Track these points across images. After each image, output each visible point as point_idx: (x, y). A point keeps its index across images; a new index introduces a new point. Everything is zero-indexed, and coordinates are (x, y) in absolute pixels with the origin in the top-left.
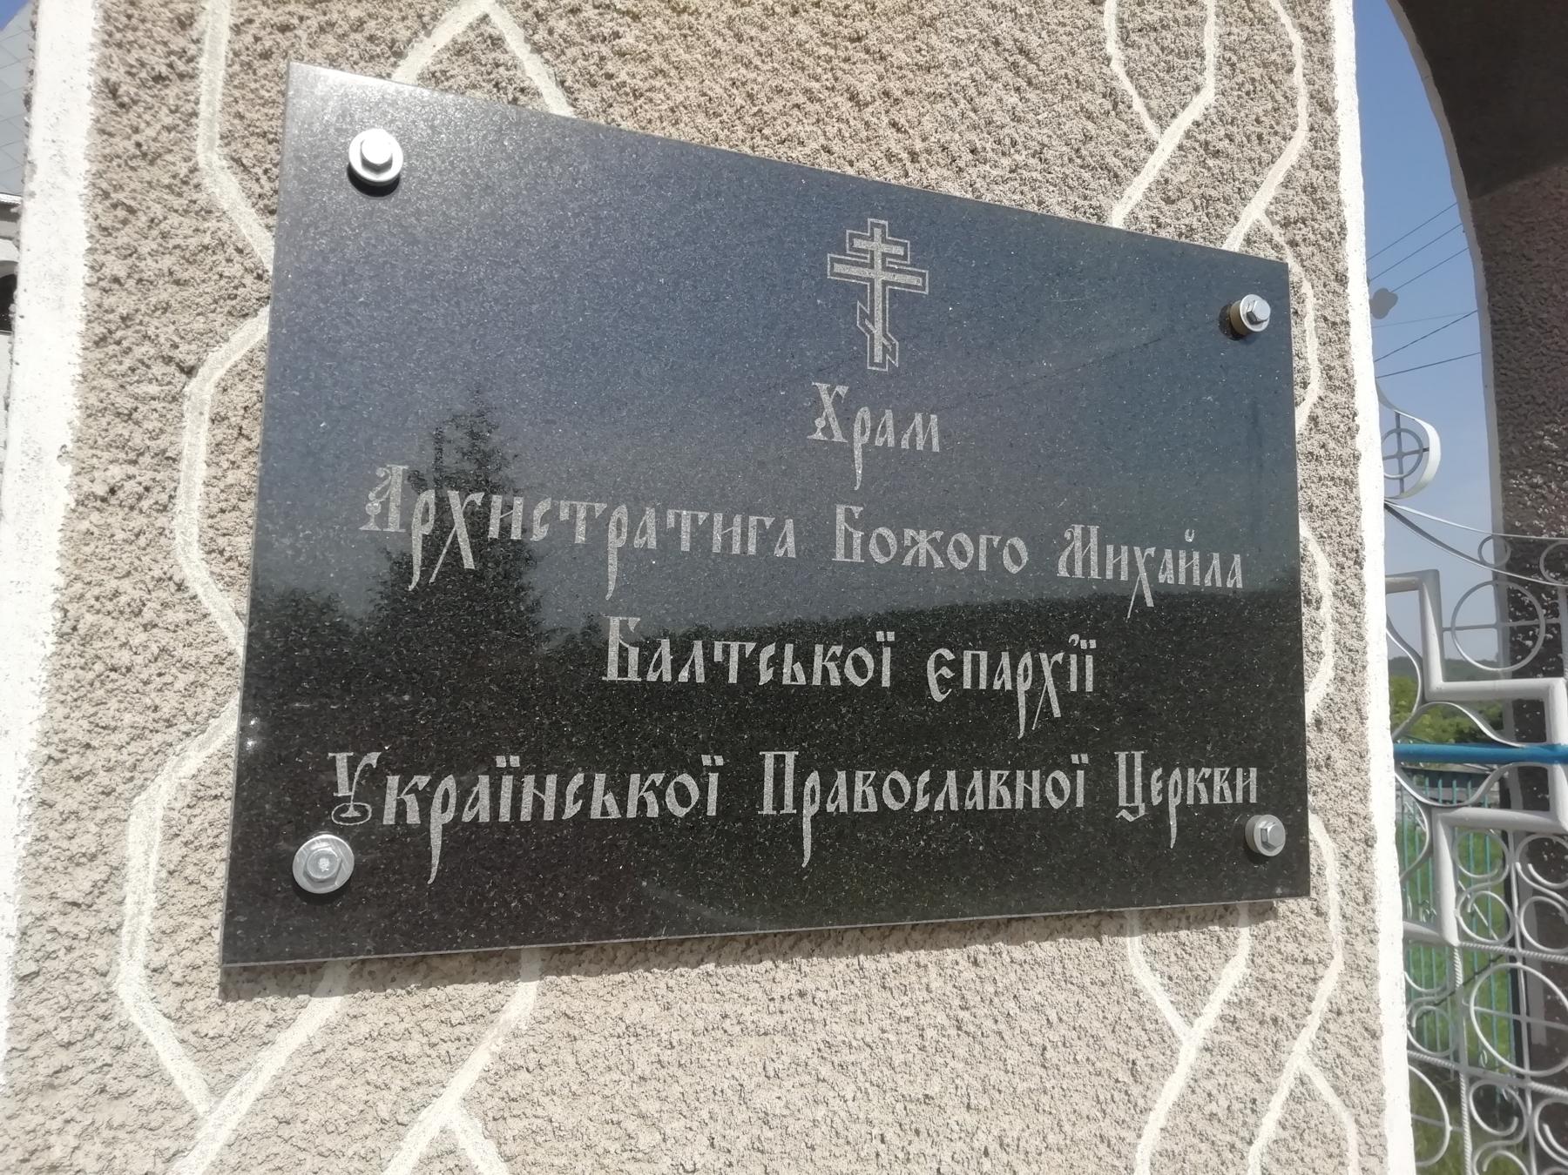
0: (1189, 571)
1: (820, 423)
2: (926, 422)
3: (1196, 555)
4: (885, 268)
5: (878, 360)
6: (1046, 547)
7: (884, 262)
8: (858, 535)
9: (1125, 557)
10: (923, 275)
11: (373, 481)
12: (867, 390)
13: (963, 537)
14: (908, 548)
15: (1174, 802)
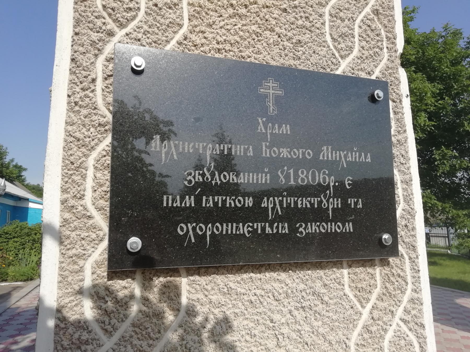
0: (356, 158)
1: (259, 128)
2: (286, 126)
3: (357, 153)
4: (273, 90)
5: (271, 112)
6: (317, 152)
7: (273, 88)
8: (268, 150)
9: (338, 154)
10: (282, 91)
11: (152, 139)
12: (271, 119)
13: (295, 150)
14: (281, 153)
15: (331, 207)
